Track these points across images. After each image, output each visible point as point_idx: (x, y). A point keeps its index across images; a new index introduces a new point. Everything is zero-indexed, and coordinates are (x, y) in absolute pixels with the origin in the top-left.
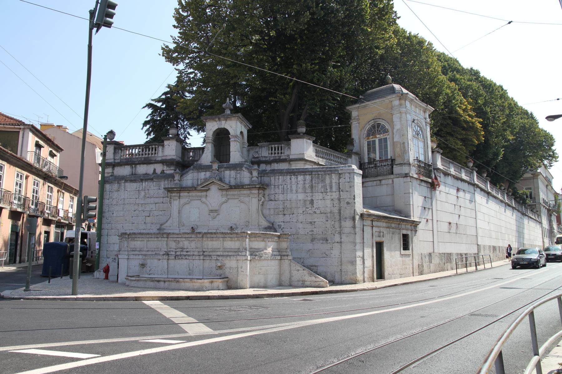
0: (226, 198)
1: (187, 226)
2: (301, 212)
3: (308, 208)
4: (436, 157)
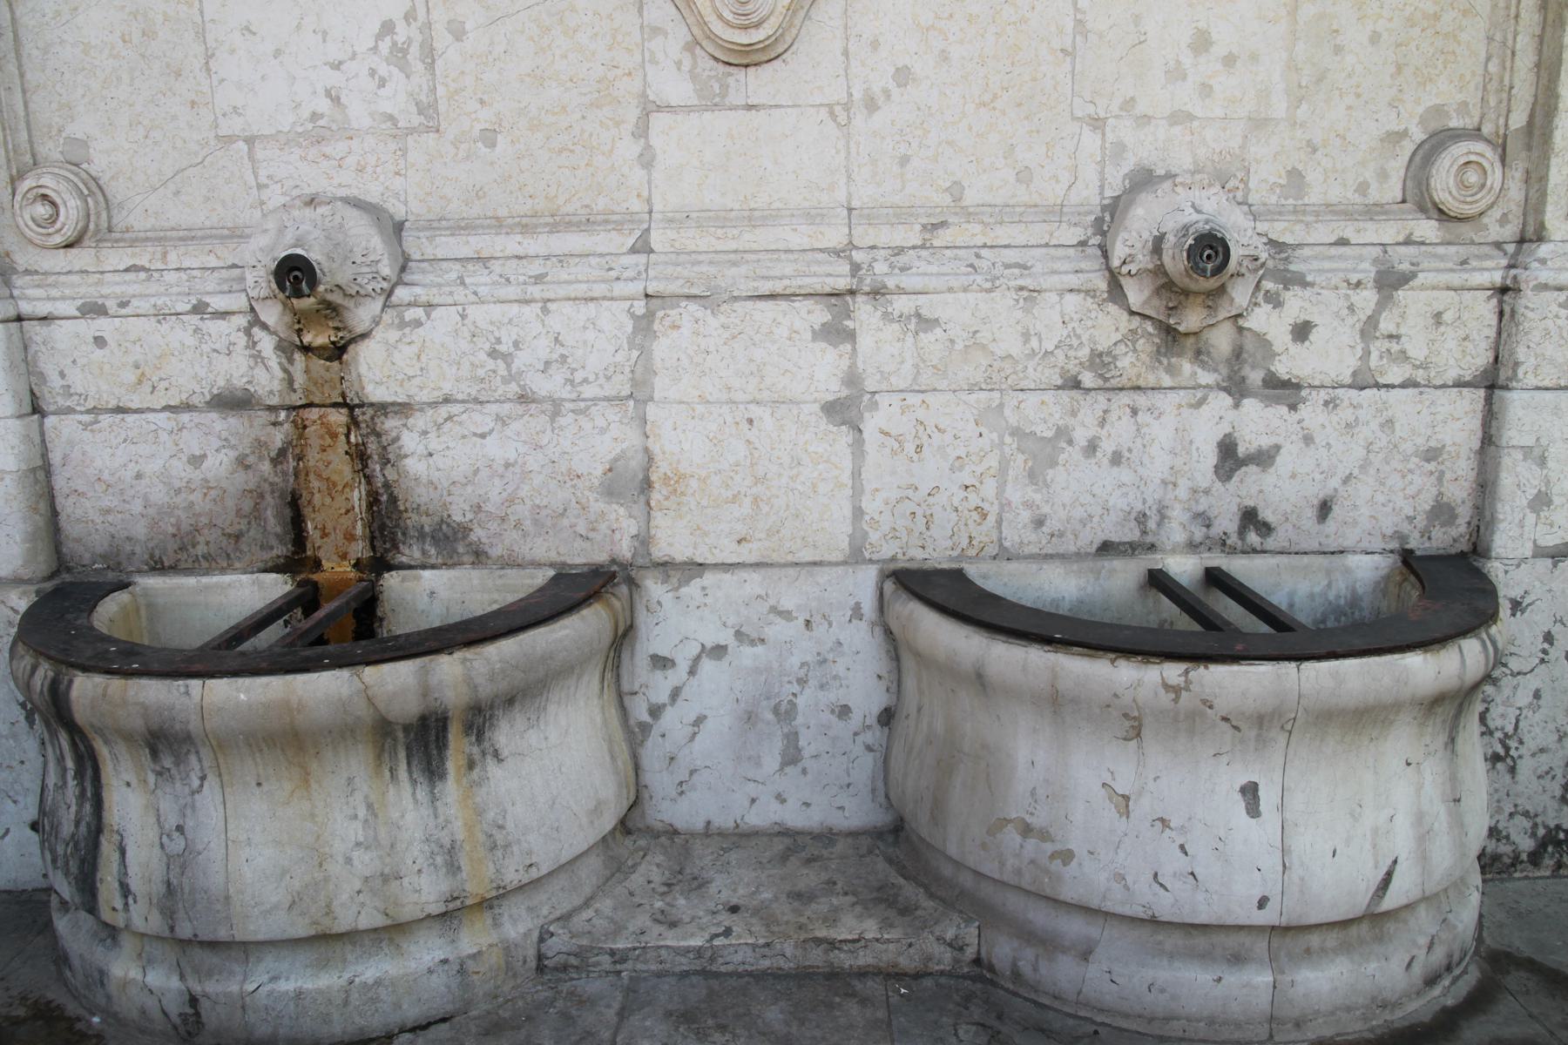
1: (161, 239)
4: (408, 635)
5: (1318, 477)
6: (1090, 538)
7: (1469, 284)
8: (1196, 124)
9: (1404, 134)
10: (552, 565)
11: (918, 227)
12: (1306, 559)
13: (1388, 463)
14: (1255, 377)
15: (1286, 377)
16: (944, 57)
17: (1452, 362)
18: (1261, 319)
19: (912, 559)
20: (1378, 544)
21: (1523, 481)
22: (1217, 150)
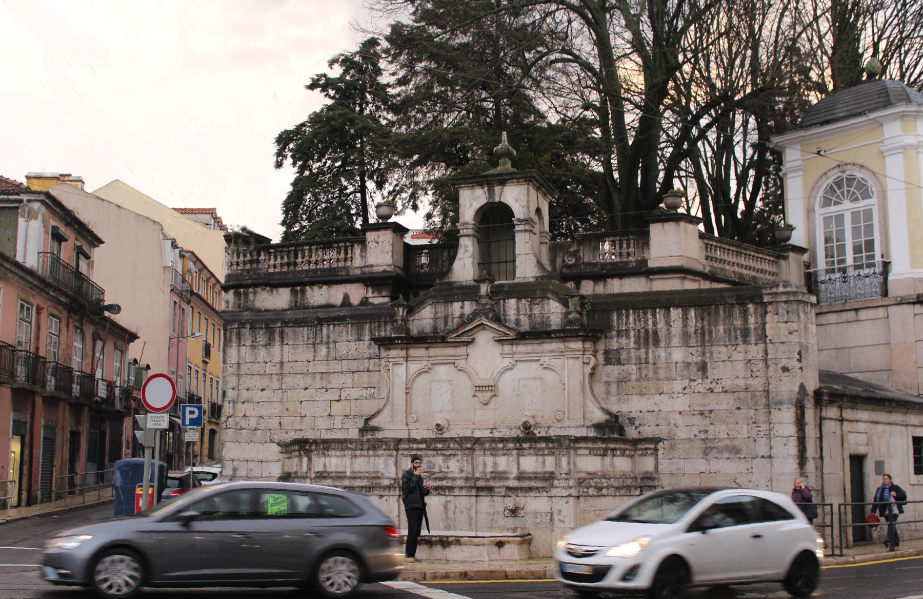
0: (510, 360)
2: (680, 389)
3: (694, 381)
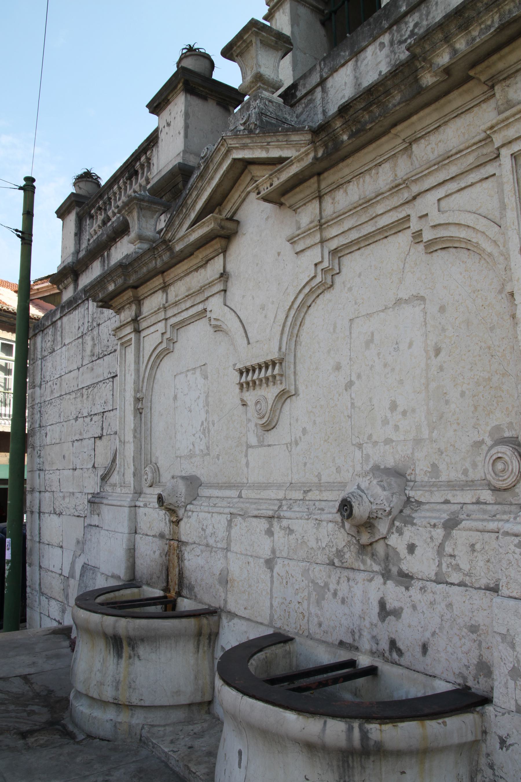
5: (420, 629)
6: (335, 638)
7: (486, 529)
8: (394, 444)
9: (482, 442)
10: (208, 605)
11: (302, 492)
12: (416, 675)
13: (452, 629)
14: (394, 570)
15: (407, 572)
16: (315, 423)
17: (483, 574)
18: (394, 540)
19: (285, 630)
20: (452, 678)
21: (504, 657)
22: (403, 456)
